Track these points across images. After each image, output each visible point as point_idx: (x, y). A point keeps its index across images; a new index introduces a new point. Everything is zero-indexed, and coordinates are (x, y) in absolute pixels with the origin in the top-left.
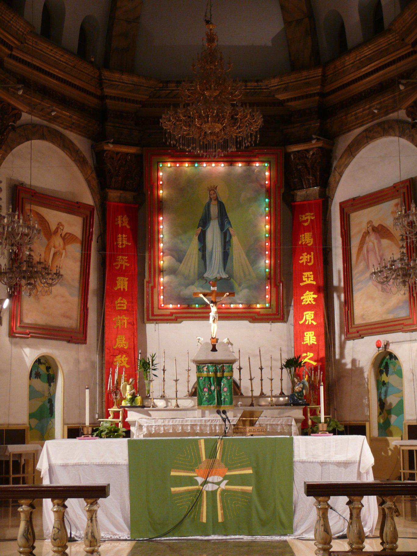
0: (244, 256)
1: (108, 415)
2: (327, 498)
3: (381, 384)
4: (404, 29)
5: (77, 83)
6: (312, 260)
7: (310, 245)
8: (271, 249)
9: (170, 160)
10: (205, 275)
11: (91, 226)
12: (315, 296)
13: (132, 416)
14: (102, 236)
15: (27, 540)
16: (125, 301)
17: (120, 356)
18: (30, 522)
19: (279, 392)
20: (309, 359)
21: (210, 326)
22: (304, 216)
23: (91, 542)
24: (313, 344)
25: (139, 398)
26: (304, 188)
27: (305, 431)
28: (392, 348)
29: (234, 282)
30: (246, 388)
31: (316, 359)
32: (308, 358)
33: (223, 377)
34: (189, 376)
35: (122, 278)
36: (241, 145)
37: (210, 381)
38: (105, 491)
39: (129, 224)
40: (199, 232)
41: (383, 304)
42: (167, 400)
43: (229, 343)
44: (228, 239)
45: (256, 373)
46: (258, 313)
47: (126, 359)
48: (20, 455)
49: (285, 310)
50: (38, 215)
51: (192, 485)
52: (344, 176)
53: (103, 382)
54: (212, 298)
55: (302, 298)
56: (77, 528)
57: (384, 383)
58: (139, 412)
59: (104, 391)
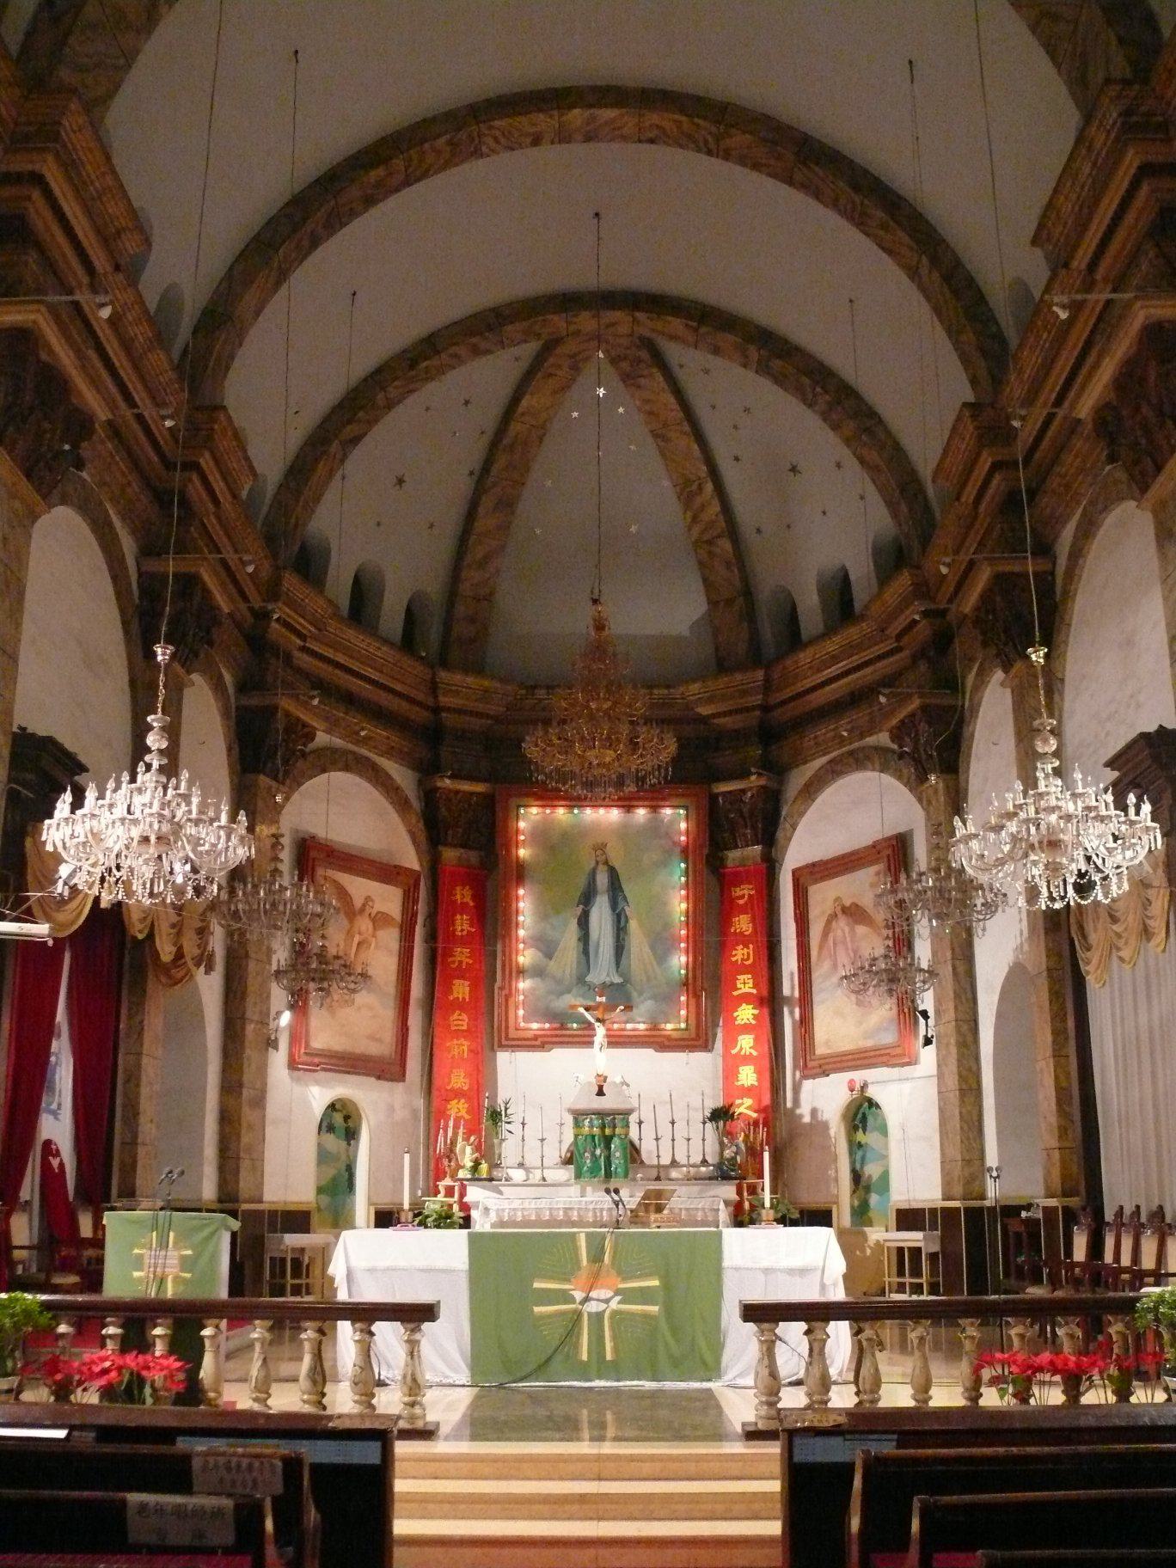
0: (647, 949)
1: (437, 1193)
2: (773, 1325)
3: (855, 1147)
5: (398, 687)
8: (687, 924)
10: (588, 979)
11: (416, 901)
12: (756, 1012)
13: (474, 1194)
14: (432, 917)
15: (314, 1382)
16: (464, 1016)
18: (318, 1356)
19: (701, 1158)
20: (747, 1108)
25: (484, 1167)
28: (871, 1092)
30: (650, 1152)
37: (594, 1140)
42: (527, 1170)
44: (622, 924)
45: (664, 1131)
46: (669, 1038)
48: (302, 1250)
51: (566, 1303)
52: (799, 828)
54: (599, 1014)
55: (736, 1014)
56: (389, 1366)
57: (860, 1145)
58: (484, 1188)
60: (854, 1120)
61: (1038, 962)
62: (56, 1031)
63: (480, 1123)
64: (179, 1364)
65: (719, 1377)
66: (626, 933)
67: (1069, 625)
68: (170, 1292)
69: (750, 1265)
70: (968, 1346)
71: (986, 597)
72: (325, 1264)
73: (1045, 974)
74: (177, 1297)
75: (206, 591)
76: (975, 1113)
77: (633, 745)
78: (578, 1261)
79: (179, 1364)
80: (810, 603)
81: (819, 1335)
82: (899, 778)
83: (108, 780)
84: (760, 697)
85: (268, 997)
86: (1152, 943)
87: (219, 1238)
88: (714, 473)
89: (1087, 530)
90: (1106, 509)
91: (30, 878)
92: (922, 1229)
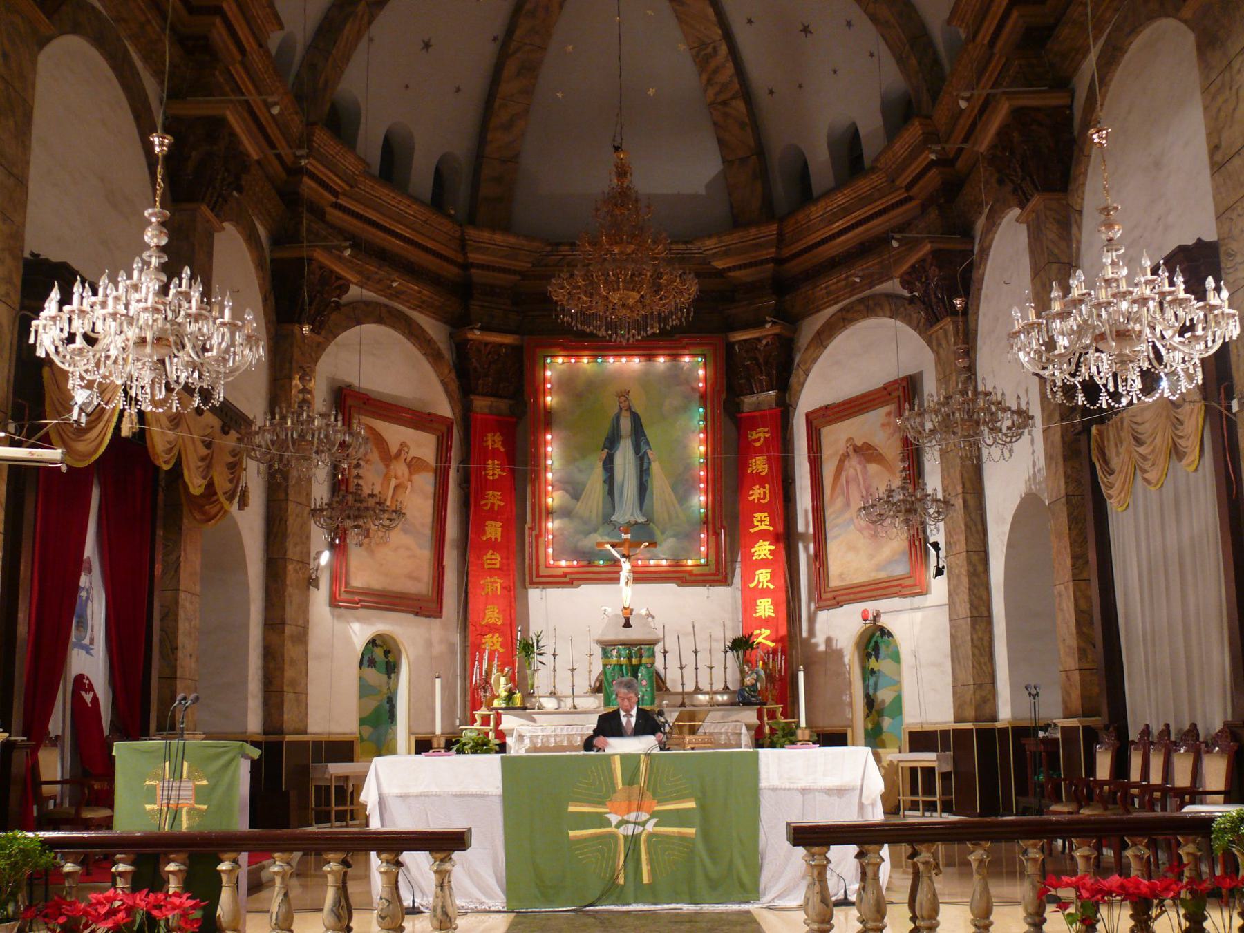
1: (474, 721)
2: (825, 849)
3: (868, 674)
4: (893, 167)
5: (430, 245)
6: (767, 496)
7: (764, 474)
9: (562, 353)
10: (613, 518)
11: (449, 449)
12: (773, 548)
13: (509, 722)
14: (465, 459)
15: (339, 917)
16: (497, 556)
17: (490, 635)
18: (343, 889)
19: (723, 686)
20: (764, 638)
21: (620, 591)
22: (754, 433)
23: (441, 922)
24: (770, 616)
25: (518, 696)
26: (754, 393)
27: (761, 742)
28: (884, 621)
29: (655, 528)
30: (674, 681)
31: (774, 638)
32: (763, 637)
33: (640, 665)
34: (590, 663)
35: (493, 523)
36: (666, 323)
37: (621, 670)
38: (464, 839)
39: (503, 445)
40: (604, 456)
41: (871, 557)
42: (559, 699)
43: (649, 615)
44: (645, 467)
45: (689, 659)
46: (690, 573)
47: (500, 640)
48: (347, 778)
49: (729, 568)
50: (370, 429)
51: (602, 826)
52: (811, 375)
53: (467, 673)
54: (624, 550)
55: (753, 550)
56: (423, 893)
57: (873, 672)
58: (518, 716)
59: (468, 685)
60: (866, 648)
61: (1053, 490)
62: (85, 565)
63: (513, 655)
64: (192, 902)
65: (758, 899)
66: (648, 475)
67: (1089, 156)
68: (185, 825)
69: (787, 785)
70: (1030, 868)
71: (1003, 133)
72: (358, 788)
73: (1064, 500)
74: (196, 830)
75: (233, 134)
76: (986, 638)
77: (657, 289)
78: (613, 784)
79: (192, 902)
80: (820, 158)
81: (872, 858)
82: (909, 323)
83: (102, 275)
84: (774, 250)
85: (308, 538)
86: (1185, 462)
87: (237, 766)
88: (728, 36)
89: (1110, 60)
90: (1134, 30)
91: (48, 407)
92: (934, 750)
